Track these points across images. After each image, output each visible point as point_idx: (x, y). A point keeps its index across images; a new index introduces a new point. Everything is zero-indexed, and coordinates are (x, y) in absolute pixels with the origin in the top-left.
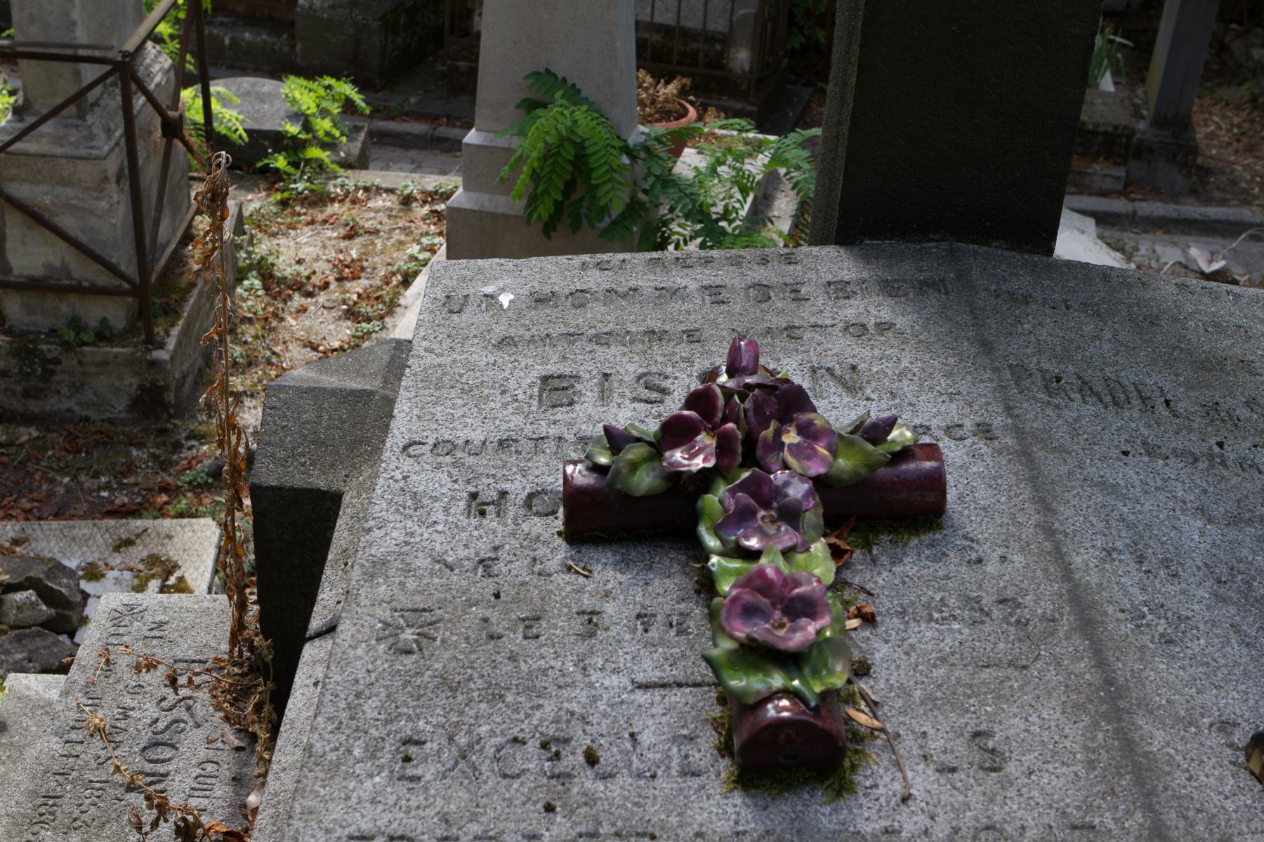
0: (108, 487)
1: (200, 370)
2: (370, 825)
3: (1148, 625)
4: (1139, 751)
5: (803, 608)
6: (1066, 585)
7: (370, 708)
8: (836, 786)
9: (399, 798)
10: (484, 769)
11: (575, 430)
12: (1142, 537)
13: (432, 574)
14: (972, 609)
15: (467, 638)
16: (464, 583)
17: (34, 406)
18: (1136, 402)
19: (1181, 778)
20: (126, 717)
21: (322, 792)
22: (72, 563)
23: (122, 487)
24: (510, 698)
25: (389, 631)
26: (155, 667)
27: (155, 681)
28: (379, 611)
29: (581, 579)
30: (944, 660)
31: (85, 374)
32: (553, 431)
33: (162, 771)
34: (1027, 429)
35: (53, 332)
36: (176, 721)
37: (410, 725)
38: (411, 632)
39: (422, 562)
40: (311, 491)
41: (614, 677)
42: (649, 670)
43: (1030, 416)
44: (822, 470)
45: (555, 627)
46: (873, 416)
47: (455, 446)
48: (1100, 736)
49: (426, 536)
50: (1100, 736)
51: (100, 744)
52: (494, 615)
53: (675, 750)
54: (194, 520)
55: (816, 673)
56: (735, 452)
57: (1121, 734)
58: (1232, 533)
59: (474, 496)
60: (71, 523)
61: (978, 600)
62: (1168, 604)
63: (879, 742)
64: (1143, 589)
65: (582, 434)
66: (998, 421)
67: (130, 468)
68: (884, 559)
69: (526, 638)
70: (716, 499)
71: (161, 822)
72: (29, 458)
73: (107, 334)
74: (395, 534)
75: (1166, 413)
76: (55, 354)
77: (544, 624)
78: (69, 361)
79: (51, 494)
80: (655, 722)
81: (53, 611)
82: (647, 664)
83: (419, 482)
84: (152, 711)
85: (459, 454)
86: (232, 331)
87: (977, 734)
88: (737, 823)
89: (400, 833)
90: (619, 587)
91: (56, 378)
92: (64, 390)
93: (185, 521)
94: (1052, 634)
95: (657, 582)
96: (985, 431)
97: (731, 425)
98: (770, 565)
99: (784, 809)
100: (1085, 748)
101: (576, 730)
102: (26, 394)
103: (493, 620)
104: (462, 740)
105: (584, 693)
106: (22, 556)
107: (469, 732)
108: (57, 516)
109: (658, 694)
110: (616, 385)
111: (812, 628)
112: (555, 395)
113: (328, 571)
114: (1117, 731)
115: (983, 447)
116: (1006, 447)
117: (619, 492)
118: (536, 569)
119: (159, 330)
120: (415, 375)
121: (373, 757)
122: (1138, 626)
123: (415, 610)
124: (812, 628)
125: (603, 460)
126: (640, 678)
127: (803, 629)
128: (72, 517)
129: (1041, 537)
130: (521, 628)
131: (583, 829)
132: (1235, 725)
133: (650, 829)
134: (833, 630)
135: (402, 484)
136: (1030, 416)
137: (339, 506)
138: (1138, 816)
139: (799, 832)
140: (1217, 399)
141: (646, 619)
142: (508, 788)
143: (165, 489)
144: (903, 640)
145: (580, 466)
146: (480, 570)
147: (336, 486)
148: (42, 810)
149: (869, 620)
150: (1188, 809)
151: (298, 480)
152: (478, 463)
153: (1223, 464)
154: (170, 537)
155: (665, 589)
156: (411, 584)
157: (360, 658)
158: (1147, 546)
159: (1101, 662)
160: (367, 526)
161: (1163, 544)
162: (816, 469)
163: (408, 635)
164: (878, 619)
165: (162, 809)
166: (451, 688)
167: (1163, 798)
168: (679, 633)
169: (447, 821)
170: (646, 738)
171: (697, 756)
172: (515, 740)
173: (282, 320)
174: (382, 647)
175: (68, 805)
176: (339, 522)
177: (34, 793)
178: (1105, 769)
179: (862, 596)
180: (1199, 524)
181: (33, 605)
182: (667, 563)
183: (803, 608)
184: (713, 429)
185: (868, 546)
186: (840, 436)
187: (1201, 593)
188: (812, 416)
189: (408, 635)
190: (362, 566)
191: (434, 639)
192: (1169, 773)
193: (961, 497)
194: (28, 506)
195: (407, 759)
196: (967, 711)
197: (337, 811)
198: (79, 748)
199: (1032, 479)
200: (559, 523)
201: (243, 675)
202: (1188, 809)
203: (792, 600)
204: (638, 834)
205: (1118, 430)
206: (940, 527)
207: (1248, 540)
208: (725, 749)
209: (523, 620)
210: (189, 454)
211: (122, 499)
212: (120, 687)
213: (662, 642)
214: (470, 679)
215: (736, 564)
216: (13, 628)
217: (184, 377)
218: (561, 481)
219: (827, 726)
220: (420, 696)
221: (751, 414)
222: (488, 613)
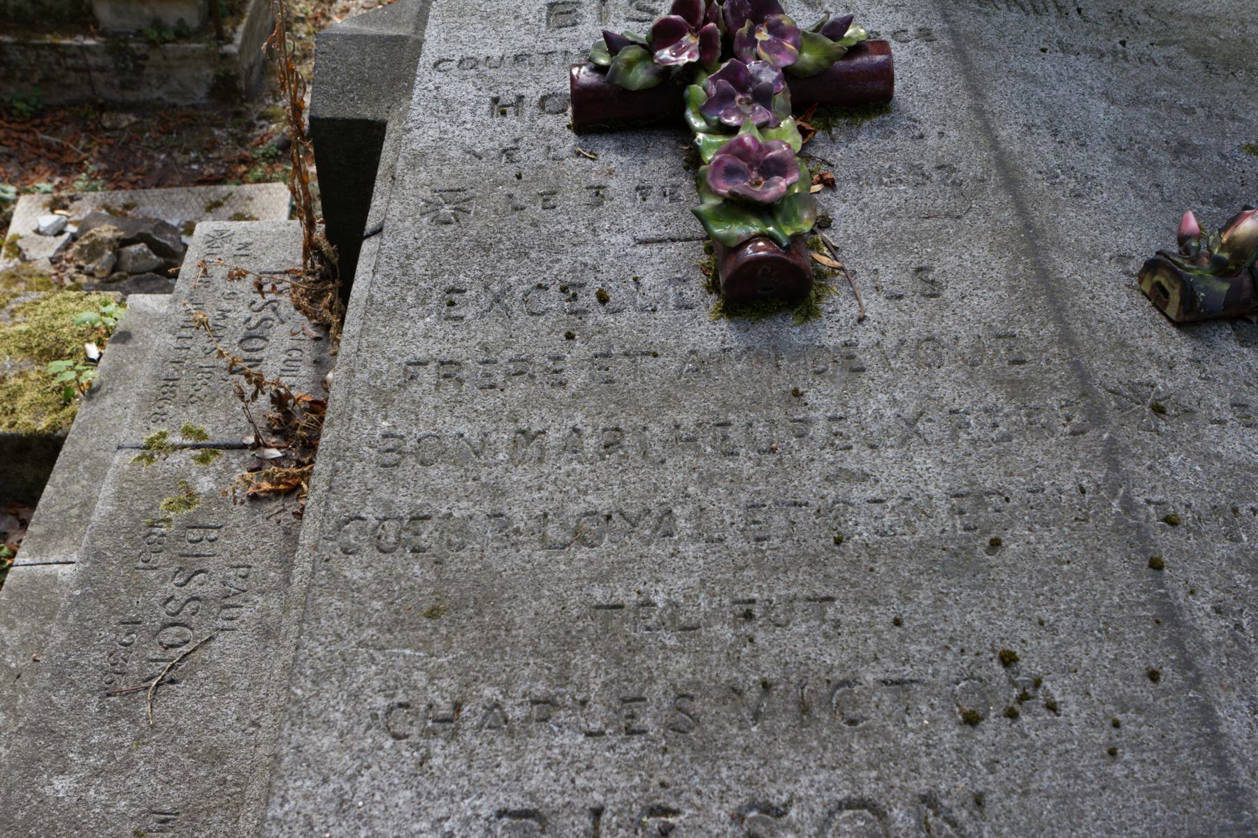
0: (197, 161)
1: (265, 62)
2: (424, 354)
3: (1061, 183)
4: (1053, 278)
5: (776, 167)
6: (993, 153)
7: (418, 267)
8: (804, 312)
9: (446, 333)
10: (514, 309)
11: (579, 45)
12: (1056, 116)
13: (463, 163)
14: (916, 174)
15: (496, 210)
16: (491, 168)
17: (131, 96)
18: (1053, 10)
19: (1085, 297)
20: (225, 317)
21: (384, 330)
22: (174, 222)
23: (208, 160)
24: (533, 255)
25: (430, 207)
26: (244, 276)
27: (246, 290)
28: (421, 193)
29: (589, 162)
30: (892, 214)
31: (169, 67)
32: (560, 47)
33: (257, 357)
34: (961, 32)
35: (139, 32)
36: (265, 319)
37: (452, 278)
38: (450, 206)
39: (455, 153)
40: (360, 121)
41: (619, 236)
42: (647, 229)
43: (964, 22)
44: (789, 62)
45: (569, 199)
46: (832, 17)
47: (478, 62)
48: (1021, 267)
49: (457, 133)
50: (1021, 267)
51: (206, 339)
52: (517, 192)
53: (671, 290)
54: (269, 185)
55: (787, 220)
56: (716, 47)
57: (1037, 265)
58: (1131, 112)
59: (495, 100)
60: (169, 190)
61: (920, 167)
62: (1077, 167)
63: (839, 278)
64: (1057, 156)
65: (585, 48)
66: (937, 26)
67: (214, 145)
68: (841, 138)
69: (544, 208)
70: (699, 90)
71: (260, 395)
72: (130, 140)
73: (185, 32)
74: (430, 133)
75: (1077, 18)
76: (143, 51)
77: (559, 197)
78: (155, 57)
79: (151, 169)
80: (654, 270)
81: (162, 260)
82: (646, 225)
83: (449, 91)
84: (246, 313)
85: (481, 68)
86: (288, 29)
87: (919, 270)
88: (723, 342)
89: (449, 359)
90: (617, 166)
91: (147, 71)
92: (154, 82)
93: (262, 185)
94: (981, 191)
95: (652, 162)
96: (925, 35)
97: (712, 25)
98: (746, 136)
99: (761, 332)
100: (1008, 277)
101: (589, 277)
102: (123, 86)
103: (517, 196)
104: (496, 288)
105: (594, 249)
106: (133, 218)
107: (501, 282)
108: (157, 186)
109: (655, 248)
110: (612, 8)
111: (783, 183)
112: (560, 18)
113: (378, 183)
114: (1034, 263)
115: (924, 47)
116: (944, 47)
117: (618, 86)
118: (550, 156)
119: (227, 28)
120: (441, 6)
121: (423, 303)
122: (1052, 184)
123: (451, 191)
124: (783, 183)
125: (603, 61)
126: (640, 236)
127: (777, 184)
128: (171, 186)
129: (972, 117)
130: (540, 201)
131: (598, 351)
132: (1131, 257)
133: (653, 349)
134: (801, 188)
135: (435, 93)
136: (964, 22)
137: (384, 133)
138: (1051, 326)
139: (774, 347)
140: (1121, 7)
141: (643, 191)
142: (535, 322)
143: (243, 161)
144: (858, 199)
145: (584, 69)
146: (504, 158)
147: (380, 116)
148: (164, 389)
149: (829, 184)
150: (1091, 320)
151: (349, 113)
152: (499, 74)
153: (1125, 58)
154: (251, 199)
155: (659, 166)
156: (447, 171)
157: (408, 229)
158: (1061, 122)
159: (1022, 211)
160: (407, 127)
161: (1074, 120)
162: (785, 61)
163: (447, 210)
164: (837, 184)
165: (259, 383)
166: (484, 249)
167: (1070, 312)
168: (672, 200)
169: (486, 349)
170: (647, 281)
171: (690, 293)
172: (540, 286)
173: (329, 19)
174: (425, 220)
175: (184, 385)
176: (385, 144)
177: (156, 377)
178: (1024, 292)
179: (824, 167)
180: (1104, 105)
181: (146, 256)
182: (660, 147)
183: (776, 167)
184: (696, 31)
185: (828, 128)
186: (804, 34)
187: (1105, 158)
188: (780, 17)
189: (447, 210)
190: (405, 158)
191: (469, 212)
192: (1076, 294)
193: (905, 87)
194: (134, 178)
195: (451, 304)
196: (911, 252)
197: (396, 345)
198: (189, 342)
199: (966, 71)
200: (568, 119)
201: (316, 282)
202: (1091, 320)
203: (766, 162)
204: (643, 354)
205: (1038, 32)
206: (888, 111)
207: (1144, 117)
208: (713, 287)
209: (542, 195)
210: (261, 132)
211: (209, 170)
212: (218, 294)
213: (658, 208)
214: (500, 241)
215: (720, 139)
216: (131, 274)
217: (251, 68)
218: (569, 86)
219: (796, 262)
220: (459, 256)
221: (728, 14)
222: (512, 191)
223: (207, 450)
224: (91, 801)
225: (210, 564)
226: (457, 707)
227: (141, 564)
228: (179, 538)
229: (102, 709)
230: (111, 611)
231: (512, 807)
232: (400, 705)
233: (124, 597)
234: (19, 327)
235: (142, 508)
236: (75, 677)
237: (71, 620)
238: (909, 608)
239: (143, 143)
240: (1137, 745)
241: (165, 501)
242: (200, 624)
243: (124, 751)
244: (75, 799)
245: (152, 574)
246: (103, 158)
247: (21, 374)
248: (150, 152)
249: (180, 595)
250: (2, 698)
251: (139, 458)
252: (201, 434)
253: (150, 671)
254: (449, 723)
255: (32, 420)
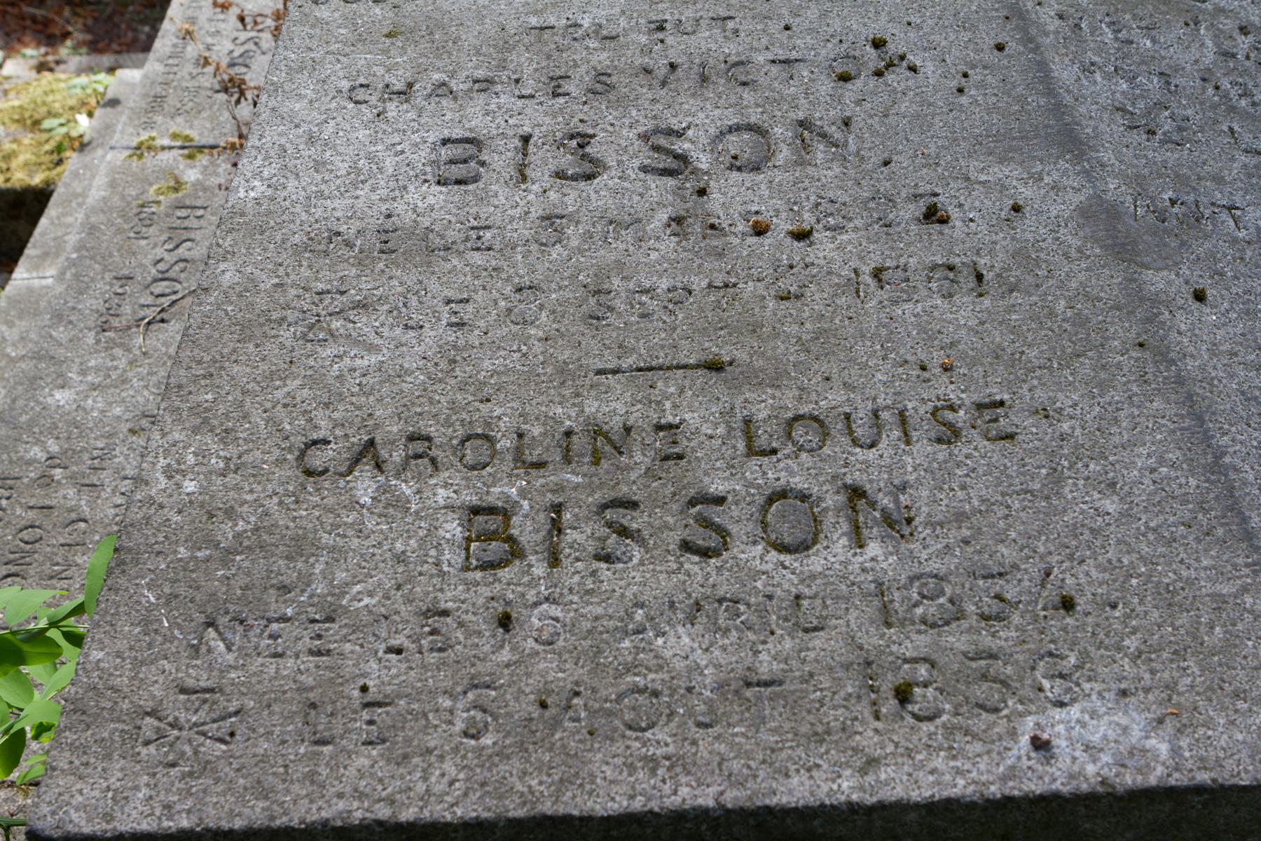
36: (247, 51)
72: (114, 13)
79: (135, 40)
84: (230, 46)
175: (172, 101)
177: (147, 95)
198: (175, 69)
223: (193, 150)
224: (88, 408)
225: (197, 235)
226: (410, 85)
227: (132, 235)
228: (167, 215)
229: (98, 342)
230: (105, 269)
231: (454, 136)
232: (362, 86)
233: (117, 259)
234: (11, 103)
235: (134, 193)
236: (73, 318)
237: (68, 275)
238: (798, 20)
239: (128, 16)
240: (982, 85)
241: (155, 187)
242: (187, 279)
243: (119, 372)
244: (74, 406)
245: (143, 242)
246: (87, 29)
247: (15, 141)
248: (134, 25)
249: (170, 258)
250: (3, 379)
251: (130, 156)
252: (187, 138)
253: (141, 313)
254: (405, 93)
255: (22, 177)
